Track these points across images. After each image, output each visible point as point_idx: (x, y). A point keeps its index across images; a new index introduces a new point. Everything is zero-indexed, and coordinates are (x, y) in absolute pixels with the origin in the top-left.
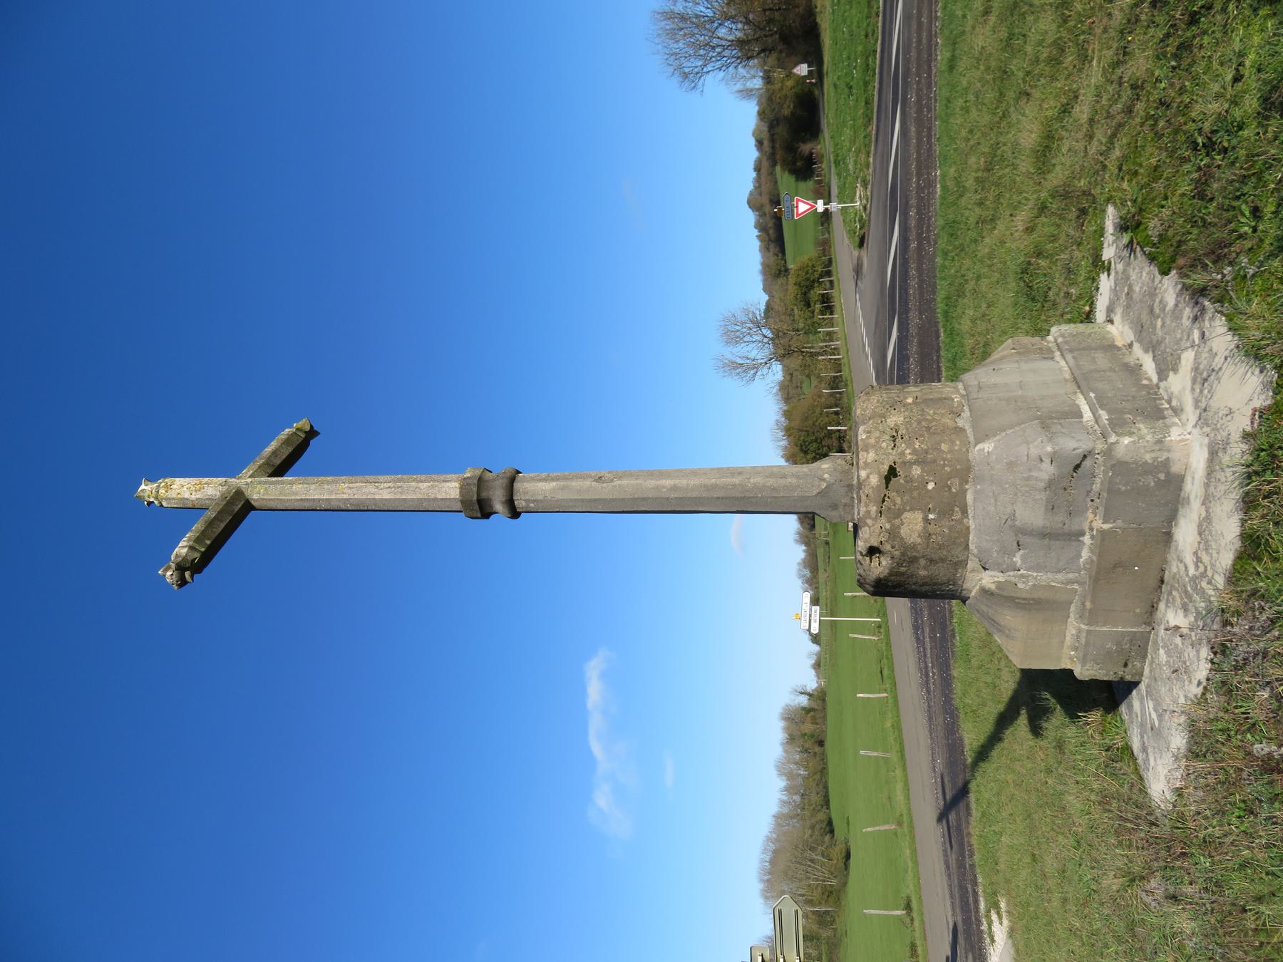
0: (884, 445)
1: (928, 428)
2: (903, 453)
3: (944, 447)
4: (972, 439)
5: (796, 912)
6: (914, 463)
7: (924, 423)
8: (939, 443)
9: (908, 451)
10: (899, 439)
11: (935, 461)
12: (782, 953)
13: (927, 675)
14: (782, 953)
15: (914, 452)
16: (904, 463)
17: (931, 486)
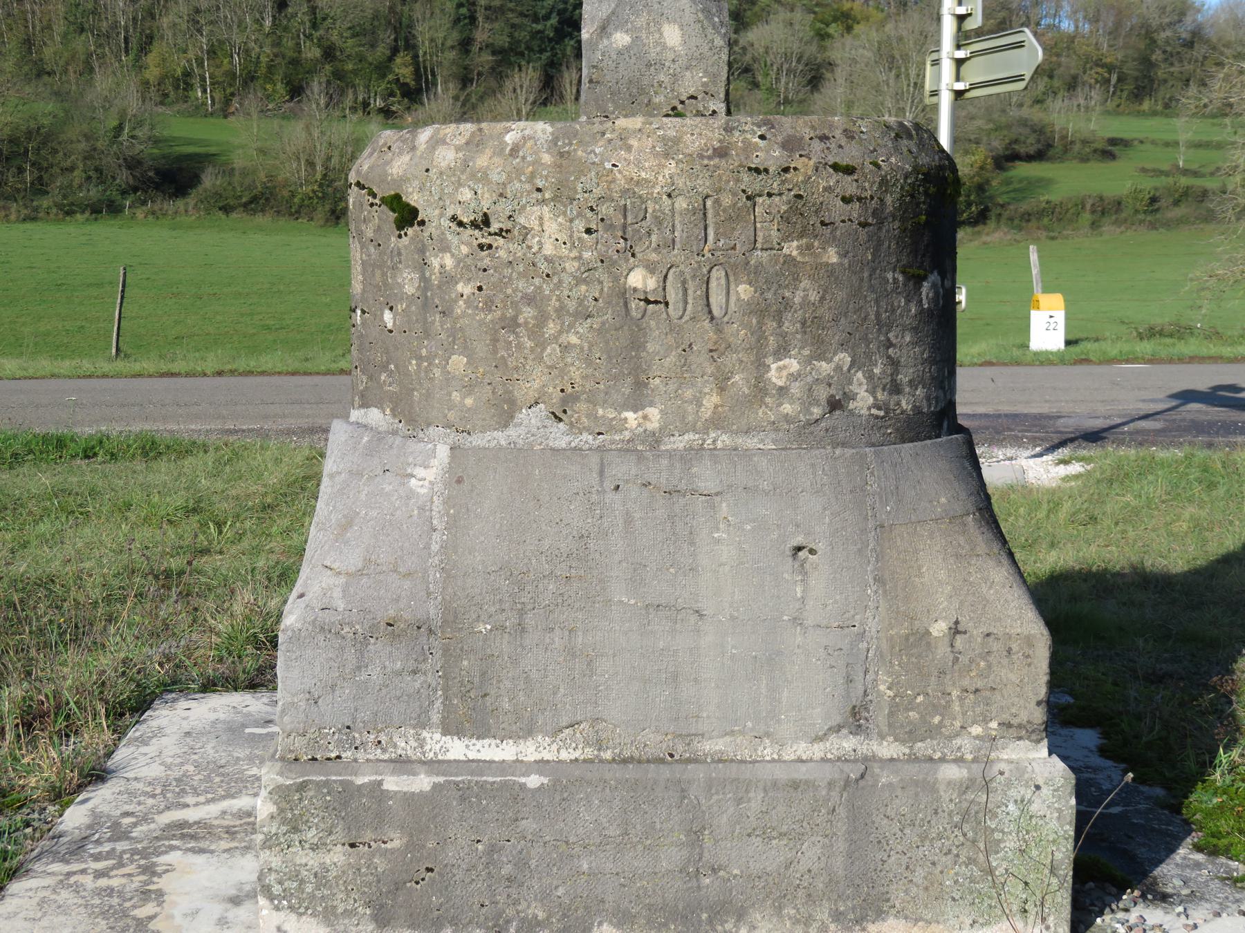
0: (466, 194)
1: (512, 324)
2: (445, 248)
3: (458, 362)
4: (478, 440)
5: (1019, 78)
6: (423, 279)
7: (528, 313)
8: (467, 351)
9: (449, 262)
10: (481, 237)
11: (427, 334)
12: (975, 54)
13: (685, 291)
14: (975, 54)
15: (449, 280)
16: (422, 250)
17: (388, 316)
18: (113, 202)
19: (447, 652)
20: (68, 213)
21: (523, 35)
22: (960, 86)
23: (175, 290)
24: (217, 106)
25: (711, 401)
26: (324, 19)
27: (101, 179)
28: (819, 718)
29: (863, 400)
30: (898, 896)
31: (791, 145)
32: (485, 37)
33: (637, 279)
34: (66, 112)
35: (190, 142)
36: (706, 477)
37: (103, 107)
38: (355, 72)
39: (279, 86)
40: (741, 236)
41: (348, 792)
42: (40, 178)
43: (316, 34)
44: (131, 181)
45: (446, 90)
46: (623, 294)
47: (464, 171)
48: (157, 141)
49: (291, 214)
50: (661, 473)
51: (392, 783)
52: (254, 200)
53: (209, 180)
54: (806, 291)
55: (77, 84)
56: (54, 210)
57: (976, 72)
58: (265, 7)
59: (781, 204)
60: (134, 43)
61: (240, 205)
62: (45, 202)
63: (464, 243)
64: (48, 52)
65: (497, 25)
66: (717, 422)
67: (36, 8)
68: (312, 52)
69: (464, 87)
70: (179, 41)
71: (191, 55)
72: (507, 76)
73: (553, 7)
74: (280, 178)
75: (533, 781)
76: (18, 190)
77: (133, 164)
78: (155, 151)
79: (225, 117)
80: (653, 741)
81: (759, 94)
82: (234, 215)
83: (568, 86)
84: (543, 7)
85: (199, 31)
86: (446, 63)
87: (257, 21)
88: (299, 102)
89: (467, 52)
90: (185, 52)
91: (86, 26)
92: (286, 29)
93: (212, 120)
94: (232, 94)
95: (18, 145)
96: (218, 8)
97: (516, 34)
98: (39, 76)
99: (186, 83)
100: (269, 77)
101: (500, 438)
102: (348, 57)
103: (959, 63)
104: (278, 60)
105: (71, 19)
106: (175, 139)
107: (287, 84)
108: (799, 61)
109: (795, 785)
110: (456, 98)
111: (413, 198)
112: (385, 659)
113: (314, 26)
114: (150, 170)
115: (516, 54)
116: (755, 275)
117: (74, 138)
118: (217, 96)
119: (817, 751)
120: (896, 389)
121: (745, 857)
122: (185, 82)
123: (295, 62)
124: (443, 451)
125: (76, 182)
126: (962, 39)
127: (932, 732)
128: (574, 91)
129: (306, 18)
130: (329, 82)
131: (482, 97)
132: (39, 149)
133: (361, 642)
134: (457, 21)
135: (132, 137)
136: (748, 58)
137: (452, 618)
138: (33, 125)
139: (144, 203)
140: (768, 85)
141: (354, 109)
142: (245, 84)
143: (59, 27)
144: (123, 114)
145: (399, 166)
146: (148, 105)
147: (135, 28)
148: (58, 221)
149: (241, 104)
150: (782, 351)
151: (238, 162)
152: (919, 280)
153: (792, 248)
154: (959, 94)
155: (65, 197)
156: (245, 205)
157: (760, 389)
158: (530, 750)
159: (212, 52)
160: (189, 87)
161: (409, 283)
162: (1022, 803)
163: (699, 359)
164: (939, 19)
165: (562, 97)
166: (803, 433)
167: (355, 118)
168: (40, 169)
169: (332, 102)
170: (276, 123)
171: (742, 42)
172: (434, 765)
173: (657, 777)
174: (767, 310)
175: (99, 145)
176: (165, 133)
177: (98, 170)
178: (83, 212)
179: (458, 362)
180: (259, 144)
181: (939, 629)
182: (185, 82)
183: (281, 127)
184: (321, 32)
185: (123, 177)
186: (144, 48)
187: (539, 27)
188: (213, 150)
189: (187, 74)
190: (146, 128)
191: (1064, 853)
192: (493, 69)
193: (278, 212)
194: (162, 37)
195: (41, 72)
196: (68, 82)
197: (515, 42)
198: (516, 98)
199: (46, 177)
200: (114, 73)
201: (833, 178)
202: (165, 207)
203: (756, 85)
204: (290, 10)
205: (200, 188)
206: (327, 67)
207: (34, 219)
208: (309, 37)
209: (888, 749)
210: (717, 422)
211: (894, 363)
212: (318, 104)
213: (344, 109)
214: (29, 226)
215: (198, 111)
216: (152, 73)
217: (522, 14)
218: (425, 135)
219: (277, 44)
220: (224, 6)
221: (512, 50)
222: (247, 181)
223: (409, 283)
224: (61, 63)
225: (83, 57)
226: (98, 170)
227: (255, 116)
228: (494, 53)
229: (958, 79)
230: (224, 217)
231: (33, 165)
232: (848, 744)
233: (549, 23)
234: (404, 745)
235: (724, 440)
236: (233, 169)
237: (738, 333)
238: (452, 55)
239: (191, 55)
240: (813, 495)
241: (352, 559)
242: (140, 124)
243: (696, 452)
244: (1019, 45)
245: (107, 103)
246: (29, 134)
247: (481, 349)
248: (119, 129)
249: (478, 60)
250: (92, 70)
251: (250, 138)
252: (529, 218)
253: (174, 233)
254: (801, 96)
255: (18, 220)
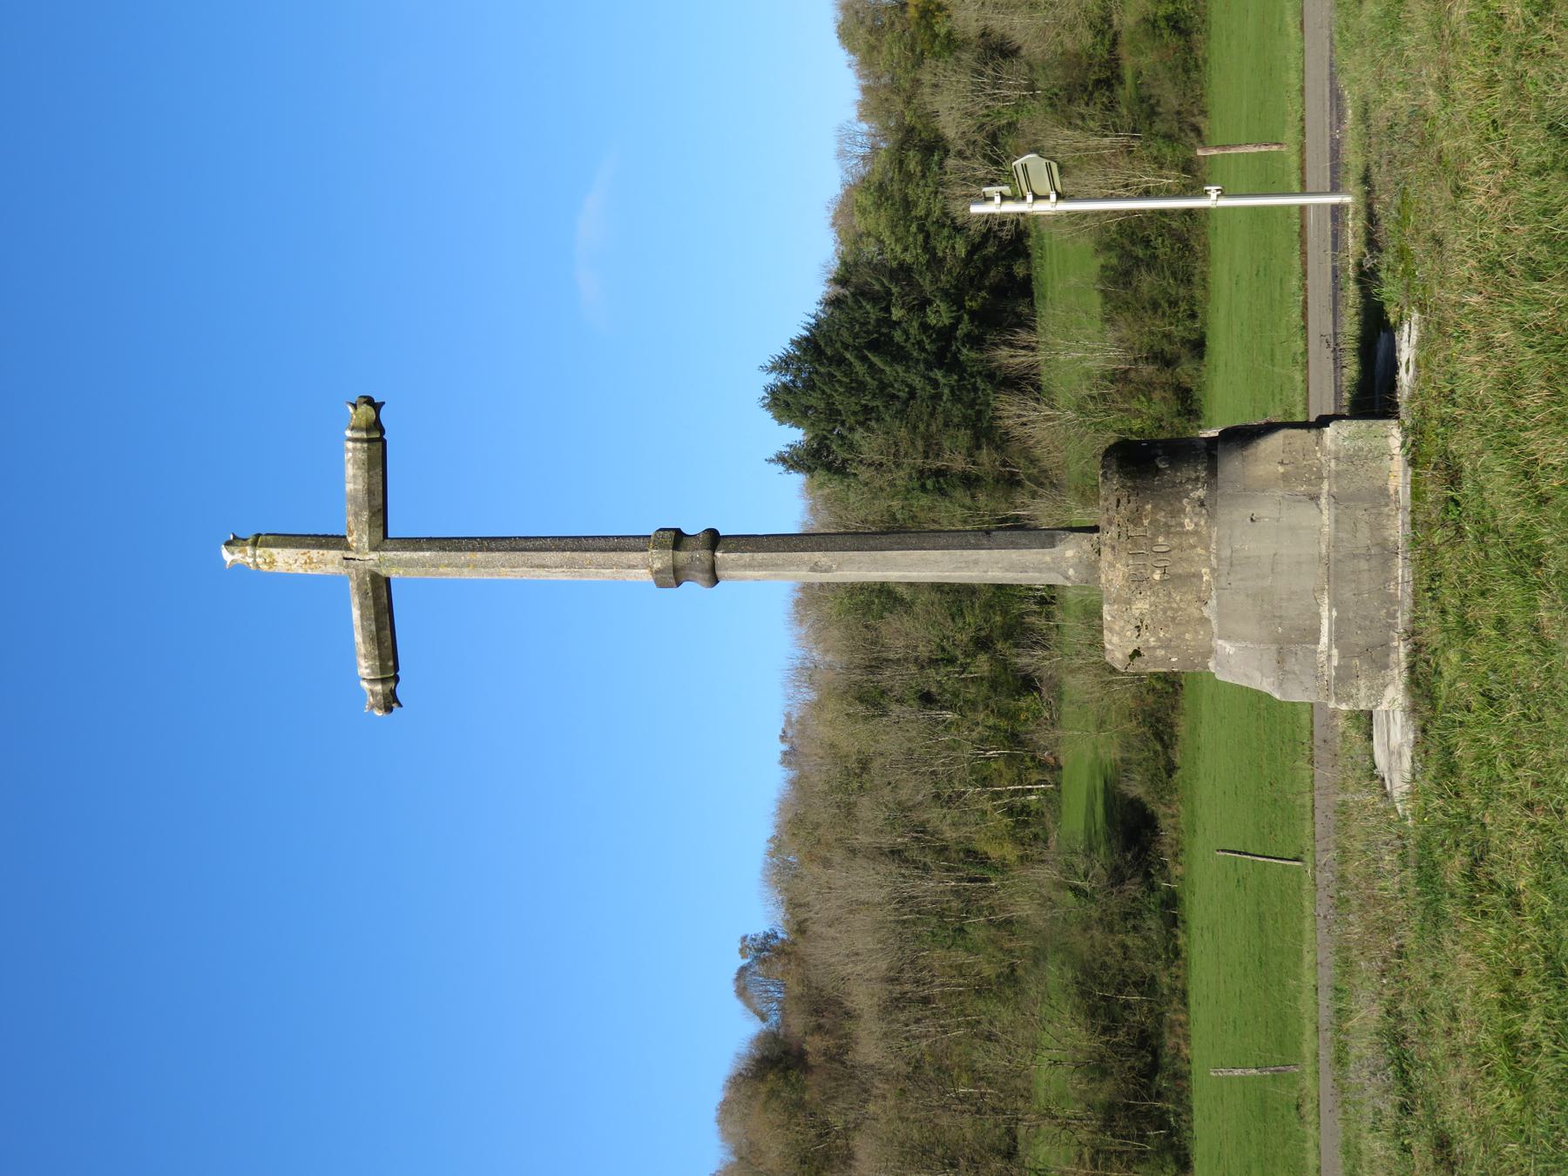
1: (1173, 619)
3: (1187, 636)
5: (1049, 168)
7: (1169, 613)
15: (1159, 639)
18: (1163, 901)
19: (1291, 642)
20: (1177, 954)
21: (957, 411)
22: (1053, 197)
23: (1266, 831)
24: (1047, 778)
25: (1199, 550)
26: (943, 649)
27: (1137, 915)
28: (1313, 511)
29: (1201, 493)
30: (1380, 483)
31: (1110, 523)
32: (960, 458)
33: (1157, 577)
34: (1057, 950)
35: (1091, 810)
36: (1226, 553)
37: (1052, 908)
38: (1005, 613)
39: (1022, 704)
40: (1142, 541)
41: (1338, 678)
42: (1136, 984)
43: (961, 659)
44: (1138, 879)
45: (1024, 506)
46: (1162, 581)
47: (1120, 634)
48: (1090, 849)
49: (1176, 693)
50: (1225, 569)
51: (1335, 662)
52: (1159, 736)
53: (1136, 788)
54: (1161, 516)
55: (1024, 939)
56: (1173, 969)
57: (1043, 186)
58: (931, 718)
59: (1131, 527)
60: (975, 872)
61: (1165, 753)
62: (1165, 980)
63: (1146, 634)
64: (988, 971)
65: (946, 444)
66: (1207, 548)
67: (937, 982)
68: (982, 665)
69: (1019, 483)
70: (972, 819)
71: (988, 806)
72: (1007, 433)
73: (923, 376)
74: (1132, 705)
75: (1334, 613)
76: (1151, 1010)
77: (1117, 877)
78: (1102, 850)
79: (1060, 768)
80: (1322, 571)
81: (1023, 121)
82: (1178, 761)
83: (1017, 360)
84: (923, 389)
85: (960, 795)
86: (992, 505)
87: (947, 729)
88: (1040, 680)
89: (978, 479)
90: (984, 813)
91: (957, 925)
92: (956, 695)
93: (1064, 784)
94: (1033, 759)
95: (1098, 1008)
96: (933, 773)
97: (956, 420)
98: (1016, 981)
99: (1021, 813)
100: (1012, 716)
101: (1214, 622)
102: (986, 621)
103: (1036, 197)
104: (992, 704)
105: (949, 942)
106: (1087, 829)
107: (1019, 694)
108: (981, 74)
109: (1337, 521)
110: (1034, 495)
111: (1130, 651)
112: (1291, 664)
113: (951, 661)
114: (1124, 858)
115: (979, 419)
116: (1155, 536)
117: (1089, 943)
118: (1035, 776)
119: (1326, 512)
120: (1197, 479)
121: (1364, 537)
122: (1020, 815)
123: (994, 685)
124: (1220, 642)
125: (1139, 942)
126: (1018, 197)
127: (1319, 470)
128: (1023, 352)
129: (943, 670)
130: (1017, 645)
131: (1032, 462)
132: (1102, 984)
133: (1285, 672)
134: (942, 492)
135: (1086, 876)
136: (979, 138)
137: (1276, 641)
138: (1073, 990)
139: (1164, 865)
140: (1010, 111)
141: (1049, 616)
142: (1021, 743)
143: (961, 957)
144: (1059, 886)
145: (1119, 655)
146: (1048, 856)
147: (959, 870)
148: (1186, 966)
149: (1046, 749)
150: (1182, 525)
151: (1113, 753)
152: (1158, 469)
153: (1146, 522)
154: (1060, 197)
155: (1158, 957)
156: (1166, 747)
157: (1195, 533)
158: (1325, 614)
159: (985, 782)
160: (1025, 810)
161: (1160, 653)
162: (1345, 439)
163: (1184, 555)
164: (1003, 215)
165: (1031, 367)
166: (1211, 516)
167: (1059, 615)
168: (1125, 984)
169: (1040, 642)
170: (1065, 709)
171: (960, 145)
172: (1330, 648)
173: (1335, 570)
174: (1168, 530)
175: (1096, 915)
176: (1081, 838)
177: (1125, 917)
178: (1176, 936)
179: (1187, 636)
180: (1092, 729)
181: (1281, 469)
182: (1020, 815)
183: (1072, 703)
184: (958, 653)
185: (1133, 888)
186: (981, 859)
187: (946, 391)
188: (1100, 784)
189: (1010, 811)
190: (1075, 859)
191: (1363, 424)
192: (997, 448)
193: (1173, 708)
194: (968, 838)
195: (1011, 977)
196: (1022, 949)
197: (966, 422)
198: (1033, 422)
199: (1134, 978)
200: (1011, 896)
201: (1122, 508)
202: (1168, 840)
203: (1011, 126)
204: (933, 690)
205: (1146, 799)
206: (999, 646)
207: (1184, 994)
208: (964, 667)
209: (1325, 486)
210: (1207, 548)
211: (1189, 480)
212: (1044, 658)
213: (1050, 629)
214: (1192, 1001)
215: (1053, 799)
216: (1010, 852)
217: (932, 415)
218: (1108, 646)
219: (973, 705)
220: (931, 765)
221: (974, 426)
222: (1136, 743)
223: (1160, 653)
224: (1000, 955)
225: (993, 931)
226: (1125, 917)
227: (1059, 733)
228: (979, 447)
229: (1047, 197)
230: (1180, 772)
231: (1120, 992)
232: (1323, 501)
233: (942, 381)
234: (1323, 658)
235: (1213, 546)
236: (1122, 760)
237: (1175, 541)
238: (982, 498)
239: (988, 806)
240: (1234, 514)
241: (1257, 674)
242: (1070, 866)
243: (1218, 558)
244: (1025, 167)
245: (1047, 903)
246: (1084, 994)
247: (1182, 629)
248: (1075, 890)
249: (987, 466)
250: (1009, 922)
251: (1084, 746)
252: (1137, 613)
253: (1200, 831)
254: (1025, 69)
255: (1187, 1013)
